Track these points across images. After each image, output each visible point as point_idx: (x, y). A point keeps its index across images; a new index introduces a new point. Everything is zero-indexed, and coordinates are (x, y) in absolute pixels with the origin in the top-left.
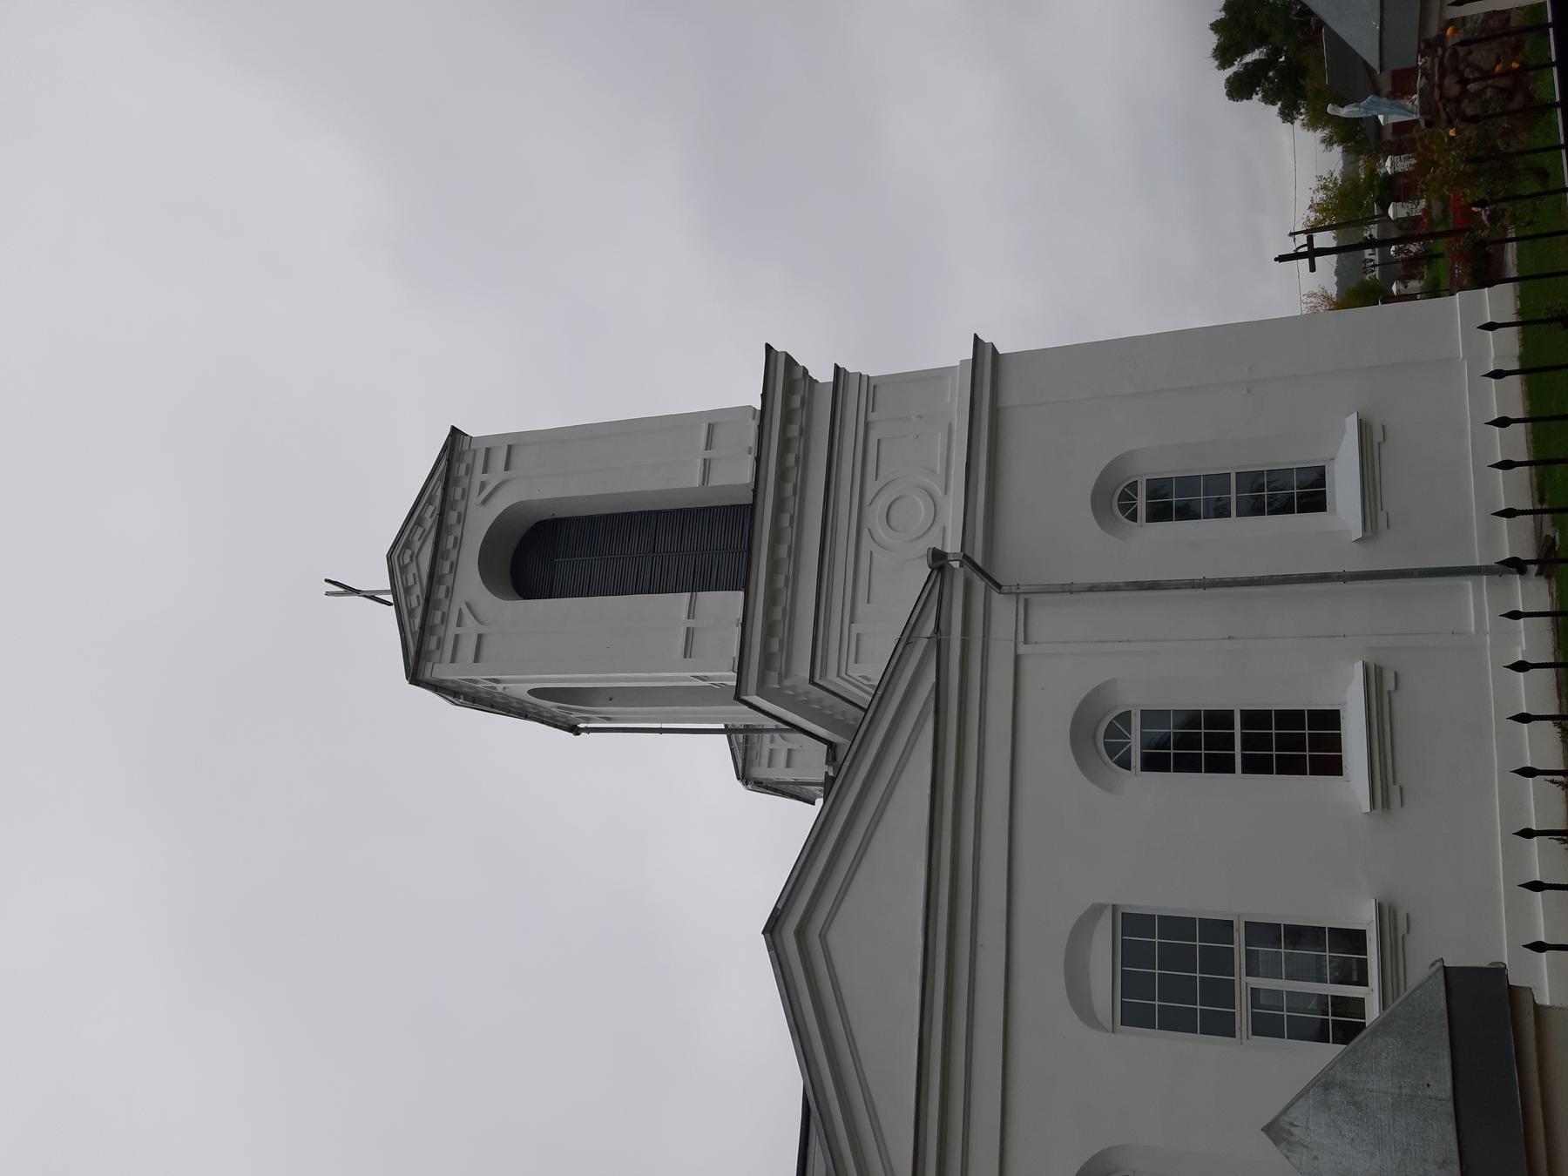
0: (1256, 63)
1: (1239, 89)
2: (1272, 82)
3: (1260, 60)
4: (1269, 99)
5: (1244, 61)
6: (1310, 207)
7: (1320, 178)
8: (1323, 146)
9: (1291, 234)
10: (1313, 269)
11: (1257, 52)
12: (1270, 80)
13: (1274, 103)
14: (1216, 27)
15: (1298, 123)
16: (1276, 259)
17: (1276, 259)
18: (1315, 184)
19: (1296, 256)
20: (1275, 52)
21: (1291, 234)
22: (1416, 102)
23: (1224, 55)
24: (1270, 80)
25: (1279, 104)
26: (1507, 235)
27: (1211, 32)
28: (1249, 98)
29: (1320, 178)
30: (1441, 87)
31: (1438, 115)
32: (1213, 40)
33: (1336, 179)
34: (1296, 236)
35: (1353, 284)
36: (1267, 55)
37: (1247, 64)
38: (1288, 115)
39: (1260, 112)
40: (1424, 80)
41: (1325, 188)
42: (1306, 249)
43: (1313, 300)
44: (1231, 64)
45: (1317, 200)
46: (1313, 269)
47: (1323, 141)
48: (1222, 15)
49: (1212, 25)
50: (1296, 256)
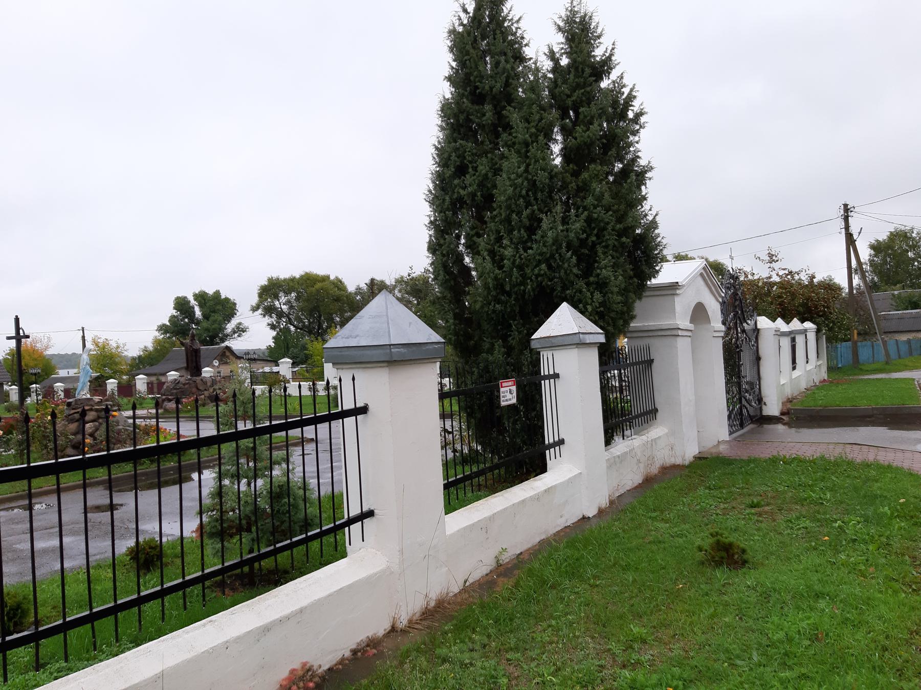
0: (194, 313)
1: (182, 305)
2: (181, 321)
3: (194, 315)
4: (172, 319)
5: (195, 306)
6: (107, 339)
7: (125, 345)
8: (143, 347)
9: (83, 328)
10: (9, 338)
11: (200, 313)
12: (183, 320)
13: (170, 321)
14: (217, 293)
15: (157, 334)
16: (17, 316)
17: (17, 316)
18: (121, 342)
19: (18, 328)
20: (198, 323)
21: (83, 328)
22: (84, 397)
23: (201, 297)
24: (183, 320)
25: (168, 324)
26: (628, 341)
27: (215, 291)
28: (175, 308)
29: (125, 345)
30: (91, 410)
31: (73, 409)
32: (210, 291)
33: (123, 353)
34: (81, 331)
35: (53, 362)
36: (197, 319)
37: (194, 308)
38: (163, 329)
39: (166, 313)
40: (97, 400)
41: (118, 347)
42: (22, 334)
43: (46, 341)
44: (195, 300)
45: (111, 342)
46: (9, 338)
47: (145, 347)
48: (223, 297)
49: (219, 291)
50: (18, 328)
